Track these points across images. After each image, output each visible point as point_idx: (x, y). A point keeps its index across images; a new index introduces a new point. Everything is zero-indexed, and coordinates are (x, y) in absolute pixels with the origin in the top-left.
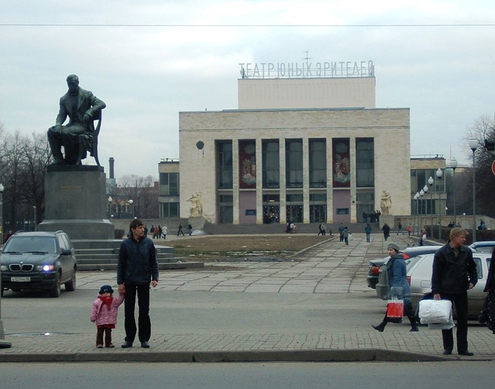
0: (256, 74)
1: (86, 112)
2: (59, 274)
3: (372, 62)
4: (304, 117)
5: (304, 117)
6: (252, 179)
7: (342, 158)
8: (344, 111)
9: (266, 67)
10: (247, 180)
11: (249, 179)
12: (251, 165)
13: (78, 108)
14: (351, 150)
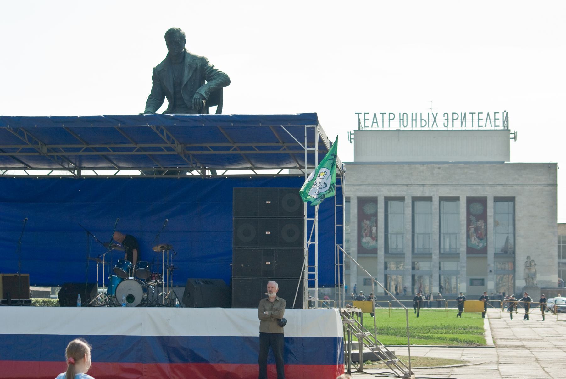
0: (375, 125)
1: (198, 91)
2: (310, 196)
3: (507, 113)
4: (434, 172)
5: (434, 172)
6: (372, 243)
7: (478, 221)
8: (481, 166)
9: (386, 117)
10: (367, 245)
11: (368, 243)
12: (371, 227)
13: (185, 83)
14: (488, 210)
